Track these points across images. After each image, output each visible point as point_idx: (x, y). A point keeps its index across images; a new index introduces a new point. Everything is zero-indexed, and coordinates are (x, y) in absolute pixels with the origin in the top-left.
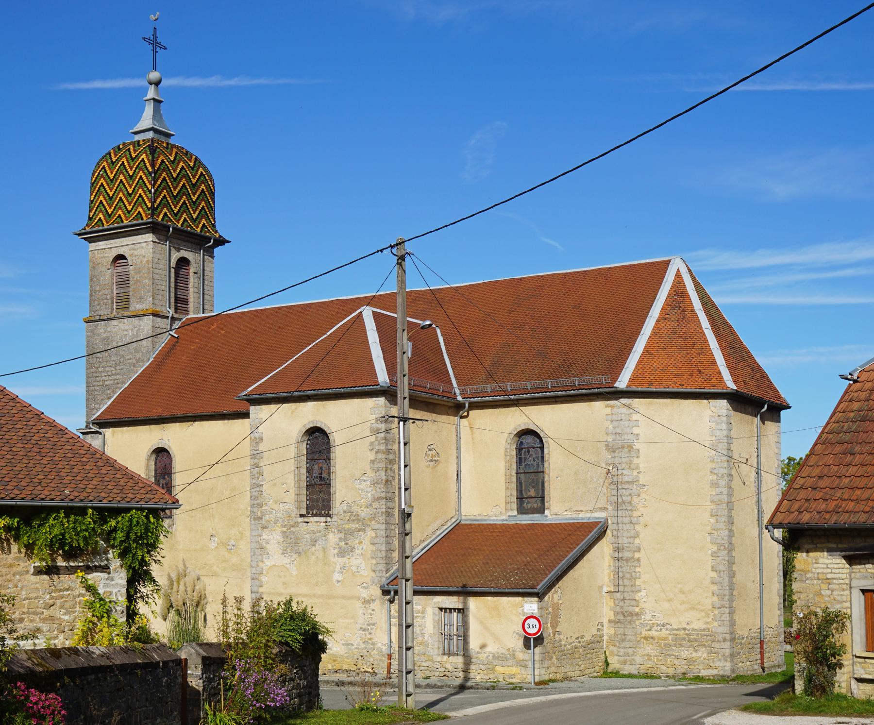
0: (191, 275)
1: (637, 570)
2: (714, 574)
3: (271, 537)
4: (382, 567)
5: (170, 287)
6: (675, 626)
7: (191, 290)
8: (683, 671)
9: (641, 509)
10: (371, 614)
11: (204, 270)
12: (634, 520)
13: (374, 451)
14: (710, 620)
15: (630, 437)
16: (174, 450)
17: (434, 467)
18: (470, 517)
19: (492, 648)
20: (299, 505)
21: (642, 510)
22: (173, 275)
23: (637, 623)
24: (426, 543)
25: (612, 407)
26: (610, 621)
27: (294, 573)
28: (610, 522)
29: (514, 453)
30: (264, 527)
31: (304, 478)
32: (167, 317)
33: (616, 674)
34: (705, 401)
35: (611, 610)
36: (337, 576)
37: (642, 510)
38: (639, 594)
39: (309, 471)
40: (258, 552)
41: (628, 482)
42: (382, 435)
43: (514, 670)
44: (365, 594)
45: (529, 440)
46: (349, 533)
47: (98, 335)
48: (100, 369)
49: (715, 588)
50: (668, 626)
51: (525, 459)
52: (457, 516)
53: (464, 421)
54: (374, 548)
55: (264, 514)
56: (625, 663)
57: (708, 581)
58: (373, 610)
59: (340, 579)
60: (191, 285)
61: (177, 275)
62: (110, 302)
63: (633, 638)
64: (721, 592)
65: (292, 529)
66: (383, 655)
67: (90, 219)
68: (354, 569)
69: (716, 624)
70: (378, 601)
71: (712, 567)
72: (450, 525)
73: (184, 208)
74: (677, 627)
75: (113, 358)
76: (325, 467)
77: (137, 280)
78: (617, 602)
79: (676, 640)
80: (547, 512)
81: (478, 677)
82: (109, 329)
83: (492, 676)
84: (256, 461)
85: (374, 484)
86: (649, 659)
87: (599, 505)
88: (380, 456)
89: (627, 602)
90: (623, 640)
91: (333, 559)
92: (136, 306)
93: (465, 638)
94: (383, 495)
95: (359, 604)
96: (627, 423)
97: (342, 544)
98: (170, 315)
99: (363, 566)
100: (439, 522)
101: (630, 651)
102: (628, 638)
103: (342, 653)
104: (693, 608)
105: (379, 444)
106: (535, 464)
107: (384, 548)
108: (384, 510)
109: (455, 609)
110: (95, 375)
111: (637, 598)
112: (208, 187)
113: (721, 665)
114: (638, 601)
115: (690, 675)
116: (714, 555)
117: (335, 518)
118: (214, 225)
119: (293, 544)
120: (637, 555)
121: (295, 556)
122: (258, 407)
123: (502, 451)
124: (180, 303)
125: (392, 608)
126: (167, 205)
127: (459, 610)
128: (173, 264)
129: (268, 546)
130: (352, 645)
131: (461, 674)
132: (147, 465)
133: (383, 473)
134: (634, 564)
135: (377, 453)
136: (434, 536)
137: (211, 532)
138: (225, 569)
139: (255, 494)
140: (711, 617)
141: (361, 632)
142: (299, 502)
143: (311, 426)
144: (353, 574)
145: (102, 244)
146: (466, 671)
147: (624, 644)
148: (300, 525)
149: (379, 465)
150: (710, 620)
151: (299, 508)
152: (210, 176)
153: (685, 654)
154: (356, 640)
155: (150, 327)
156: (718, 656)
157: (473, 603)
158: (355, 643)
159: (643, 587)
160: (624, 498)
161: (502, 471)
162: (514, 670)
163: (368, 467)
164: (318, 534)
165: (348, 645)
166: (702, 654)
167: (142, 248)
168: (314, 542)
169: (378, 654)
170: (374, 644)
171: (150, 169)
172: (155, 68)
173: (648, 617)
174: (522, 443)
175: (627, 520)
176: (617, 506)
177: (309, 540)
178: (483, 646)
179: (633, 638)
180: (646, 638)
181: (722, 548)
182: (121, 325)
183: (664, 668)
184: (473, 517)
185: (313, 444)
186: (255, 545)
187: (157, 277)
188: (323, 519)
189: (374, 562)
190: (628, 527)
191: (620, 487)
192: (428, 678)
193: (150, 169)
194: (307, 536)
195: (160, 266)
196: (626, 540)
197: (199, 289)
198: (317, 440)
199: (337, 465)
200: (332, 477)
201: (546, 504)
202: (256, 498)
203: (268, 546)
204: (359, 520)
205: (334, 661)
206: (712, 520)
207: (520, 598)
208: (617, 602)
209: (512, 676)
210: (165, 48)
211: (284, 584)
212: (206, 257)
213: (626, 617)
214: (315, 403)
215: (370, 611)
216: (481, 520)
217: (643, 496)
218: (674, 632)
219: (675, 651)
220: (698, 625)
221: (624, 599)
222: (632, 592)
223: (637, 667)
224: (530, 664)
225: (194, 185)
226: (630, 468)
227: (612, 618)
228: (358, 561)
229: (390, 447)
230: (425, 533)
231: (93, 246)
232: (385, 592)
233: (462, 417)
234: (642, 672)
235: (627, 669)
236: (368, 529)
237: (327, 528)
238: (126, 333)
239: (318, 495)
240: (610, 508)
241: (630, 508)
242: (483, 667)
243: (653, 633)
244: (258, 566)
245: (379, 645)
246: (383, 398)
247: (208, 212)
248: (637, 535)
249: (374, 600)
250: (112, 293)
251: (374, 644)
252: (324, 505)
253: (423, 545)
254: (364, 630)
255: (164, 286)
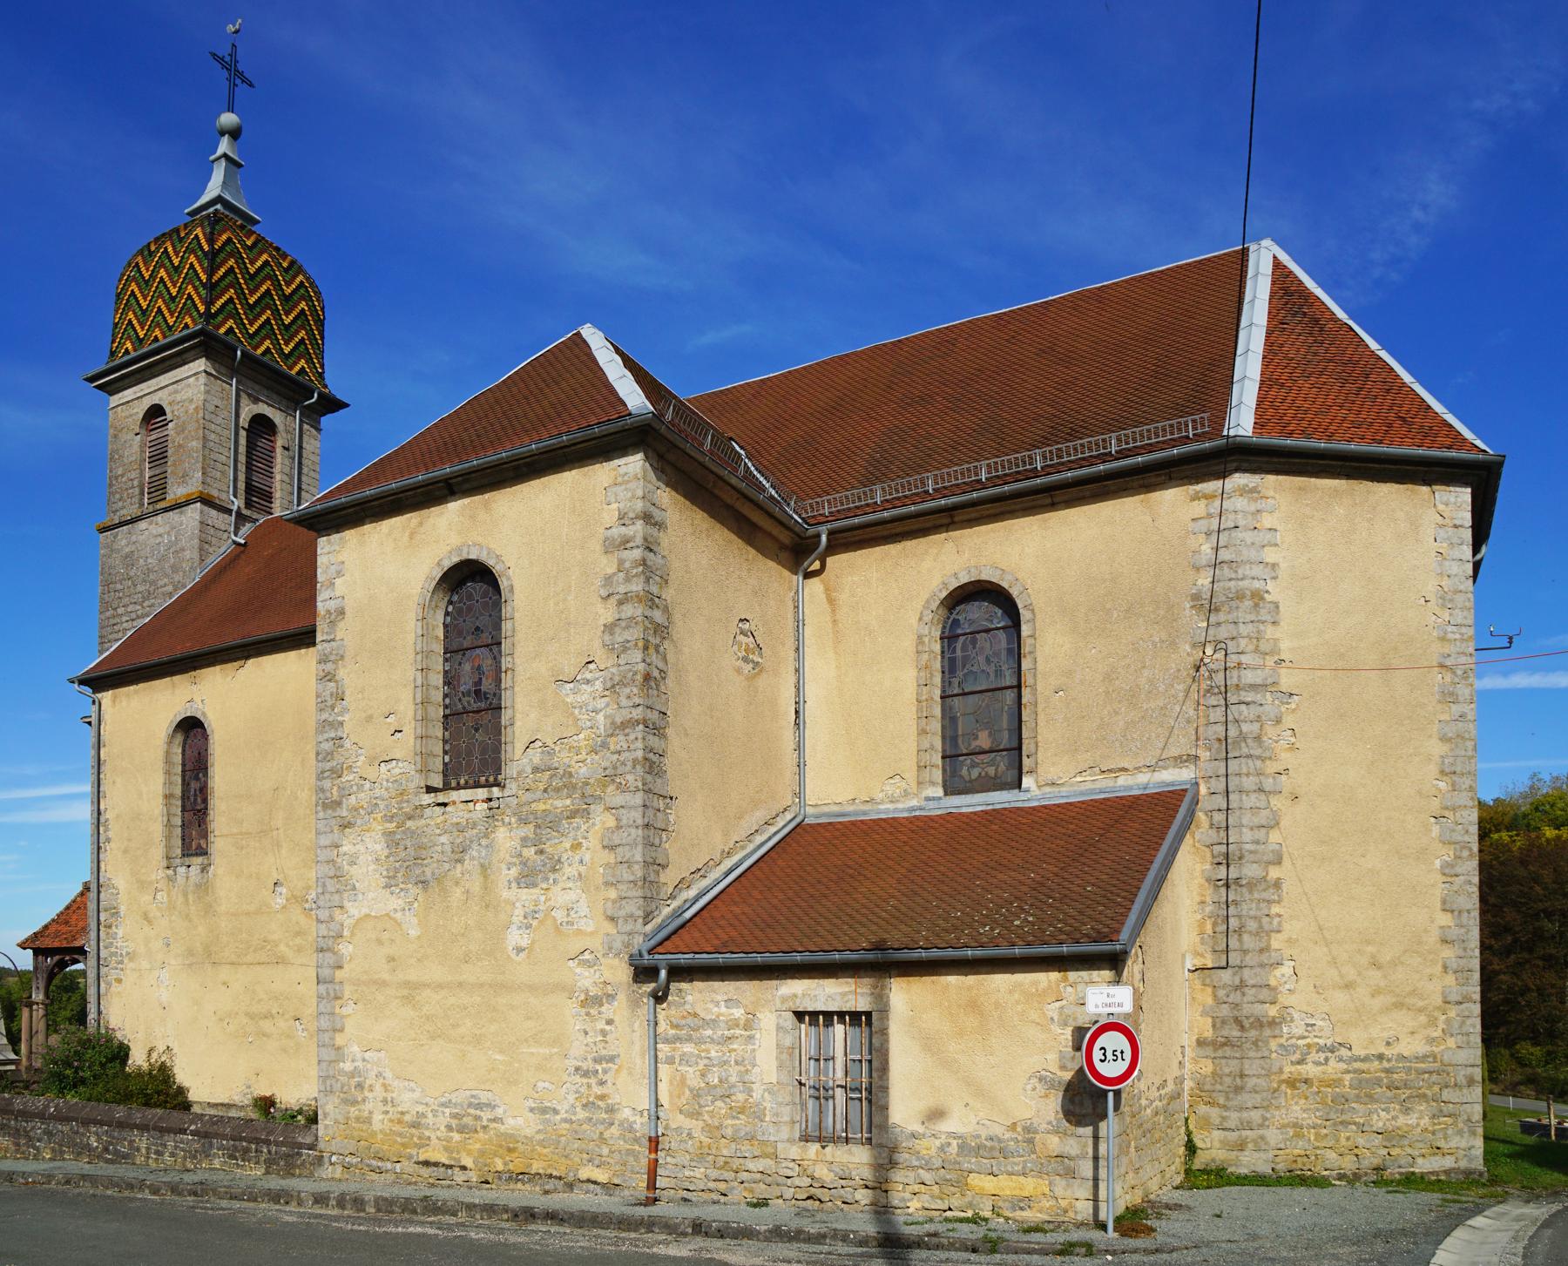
0: (279, 450)
1: (1275, 909)
2: (1446, 919)
3: (361, 847)
4: (634, 908)
5: (236, 461)
6: (1358, 1051)
7: (278, 477)
8: (1376, 1161)
9: (1283, 755)
10: (604, 1033)
11: (301, 447)
12: (1268, 784)
13: (613, 600)
14: (1438, 1033)
15: (1257, 571)
16: (212, 721)
17: (751, 678)
18: (826, 809)
19: (959, 1123)
20: (425, 763)
21: (1286, 759)
22: (243, 441)
23: (1273, 1045)
24: (735, 859)
25: (1209, 497)
26: (1201, 1043)
27: (413, 933)
28: (1203, 790)
29: (937, 647)
30: (346, 826)
31: (438, 696)
32: (229, 512)
33: (1218, 1177)
34: (1425, 489)
35: (1204, 1013)
36: (516, 937)
37: (1286, 759)
38: (1278, 972)
39: (450, 680)
40: (331, 885)
41: (1254, 687)
42: (637, 554)
43: (1030, 1185)
44: (587, 979)
45: (979, 613)
46: (547, 824)
47: (118, 551)
48: (120, 611)
49: (1448, 953)
50: (1344, 1052)
51: (965, 659)
52: (795, 809)
53: (815, 583)
54: (610, 858)
55: (345, 793)
56: (1241, 1146)
57: (1433, 938)
58: (610, 1022)
59: (524, 943)
60: (277, 469)
61: (251, 446)
62: (137, 491)
63: (1262, 1082)
64: (1462, 962)
65: (409, 824)
66: (636, 1140)
67: (113, 353)
68: (559, 915)
69: (1451, 1043)
70: (622, 997)
71: (1444, 902)
72: (782, 825)
73: (266, 330)
74: (1363, 1053)
75: (140, 588)
76: (487, 663)
77: (180, 446)
78: (1221, 993)
79: (1358, 1085)
80: (1027, 781)
81: (914, 1205)
82: (134, 538)
83: (955, 1202)
84: (329, 667)
85: (612, 688)
86: (1298, 1136)
87: (1174, 751)
88: (629, 610)
89: (1250, 992)
90: (1238, 1090)
91: (505, 894)
92: (176, 492)
93: (872, 1093)
94: (637, 714)
95: (571, 1008)
96: (1249, 537)
97: (530, 852)
98: (235, 508)
99: (583, 909)
100: (760, 815)
101: (1255, 1116)
102: (1251, 1082)
103: (529, 1132)
104: (1399, 1005)
105: (628, 580)
106: (991, 669)
107: (639, 858)
108: (640, 754)
109: (841, 1015)
110: (112, 621)
111: (1273, 982)
112: (312, 308)
113: (1463, 1144)
114: (1274, 989)
115: (1393, 1172)
116: (1448, 872)
117: (512, 787)
118: (321, 375)
119: (411, 865)
120: (1274, 873)
121: (414, 890)
122: (335, 537)
123: (909, 643)
124: (257, 495)
125: (661, 1016)
126: (235, 315)
127: (855, 1018)
128: (244, 420)
129: (354, 870)
130: (556, 1112)
131: (864, 1197)
132: (168, 753)
133: (637, 656)
134: (1265, 895)
135: (620, 603)
136: (751, 847)
137: (275, 876)
138: (299, 950)
139: (327, 746)
140: (1442, 1025)
141: (577, 1079)
142: (424, 755)
143: (456, 560)
144: (558, 928)
145: (128, 394)
146: (880, 1186)
147: (1238, 1100)
148: (428, 812)
149: (627, 635)
150: (1438, 1033)
151: (424, 770)
152: (318, 294)
153: (1380, 1120)
154: (565, 1100)
155: (197, 523)
156: (1455, 1124)
157: (903, 995)
158: (563, 1108)
159: (1287, 953)
160: (1245, 728)
161: (910, 691)
162: (1030, 1185)
163: (597, 643)
164: (470, 833)
165: (544, 1111)
166: (1417, 1119)
167: (189, 388)
168: (459, 854)
169: (622, 1137)
170: (611, 1110)
171: (206, 247)
172: (231, 109)
173: (1299, 1030)
174: (956, 623)
175: (1249, 783)
176: (1226, 748)
177: (448, 848)
178: (936, 1114)
179: (1262, 1082)
180: (1292, 1083)
181: (1465, 853)
182: (154, 530)
183: (1332, 1155)
184: (836, 809)
185: (459, 611)
186: (327, 870)
187: (213, 436)
188: (482, 793)
189: (613, 894)
190: (1251, 800)
191: (1232, 698)
192: (762, 1203)
193: (206, 247)
194: (444, 839)
195: (219, 420)
196: (1248, 835)
197: (292, 478)
198: (470, 582)
199: (519, 651)
200: (506, 681)
201: (1026, 762)
202: (329, 756)
203: (354, 870)
204: (574, 787)
205: (510, 1150)
206: (1442, 785)
207: (1054, 976)
208: (1221, 993)
209: (1025, 1202)
210: (251, 85)
211: (391, 959)
212: (306, 427)
213: (1240, 1030)
214: (466, 501)
215: (601, 1025)
216: (856, 813)
217: (1289, 721)
218: (1357, 1065)
219: (1359, 1112)
220: (1412, 1046)
221: (1241, 986)
222: (1262, 966)
223: (1271, 1154)
224: (1086, 1169)
225: (286, 299)
226: (1257, 650)
227: (1209, 1034)
228: (572, 896)
229: (655, 589)
230: (715, 842)
231: (115, 400)
232: (644, 973)
233: (808, 575)
234: (1281, 1167)
235: (1250, 1162)
236: (597, 809)
237: (493, 812)
238: (159, 540)
239: (470, 733)
240: (1204, 755)
241: (1258, 752)
242: (927, 1177)
243: (1309, 1070)
244: (332, 919)
245: (626, 1113)
246: (640, 456)
247: (313, 349)
248: (1274, 824)
249: (611, 997)
250: (142, 474)
251: (611, 1110)
252: (484, 763)
253: (728, 863)
254: (586, 1074)
255: (225, 457)
